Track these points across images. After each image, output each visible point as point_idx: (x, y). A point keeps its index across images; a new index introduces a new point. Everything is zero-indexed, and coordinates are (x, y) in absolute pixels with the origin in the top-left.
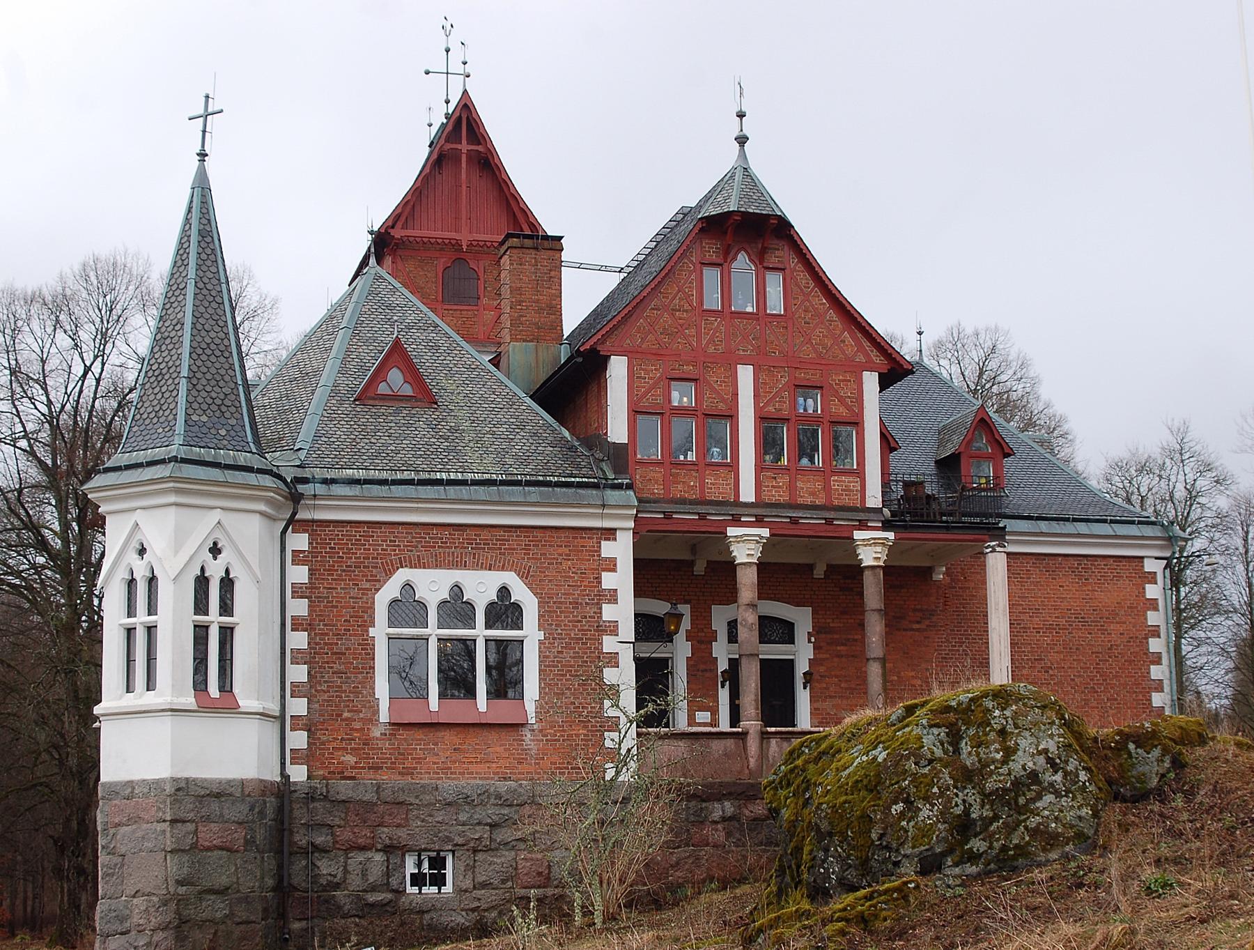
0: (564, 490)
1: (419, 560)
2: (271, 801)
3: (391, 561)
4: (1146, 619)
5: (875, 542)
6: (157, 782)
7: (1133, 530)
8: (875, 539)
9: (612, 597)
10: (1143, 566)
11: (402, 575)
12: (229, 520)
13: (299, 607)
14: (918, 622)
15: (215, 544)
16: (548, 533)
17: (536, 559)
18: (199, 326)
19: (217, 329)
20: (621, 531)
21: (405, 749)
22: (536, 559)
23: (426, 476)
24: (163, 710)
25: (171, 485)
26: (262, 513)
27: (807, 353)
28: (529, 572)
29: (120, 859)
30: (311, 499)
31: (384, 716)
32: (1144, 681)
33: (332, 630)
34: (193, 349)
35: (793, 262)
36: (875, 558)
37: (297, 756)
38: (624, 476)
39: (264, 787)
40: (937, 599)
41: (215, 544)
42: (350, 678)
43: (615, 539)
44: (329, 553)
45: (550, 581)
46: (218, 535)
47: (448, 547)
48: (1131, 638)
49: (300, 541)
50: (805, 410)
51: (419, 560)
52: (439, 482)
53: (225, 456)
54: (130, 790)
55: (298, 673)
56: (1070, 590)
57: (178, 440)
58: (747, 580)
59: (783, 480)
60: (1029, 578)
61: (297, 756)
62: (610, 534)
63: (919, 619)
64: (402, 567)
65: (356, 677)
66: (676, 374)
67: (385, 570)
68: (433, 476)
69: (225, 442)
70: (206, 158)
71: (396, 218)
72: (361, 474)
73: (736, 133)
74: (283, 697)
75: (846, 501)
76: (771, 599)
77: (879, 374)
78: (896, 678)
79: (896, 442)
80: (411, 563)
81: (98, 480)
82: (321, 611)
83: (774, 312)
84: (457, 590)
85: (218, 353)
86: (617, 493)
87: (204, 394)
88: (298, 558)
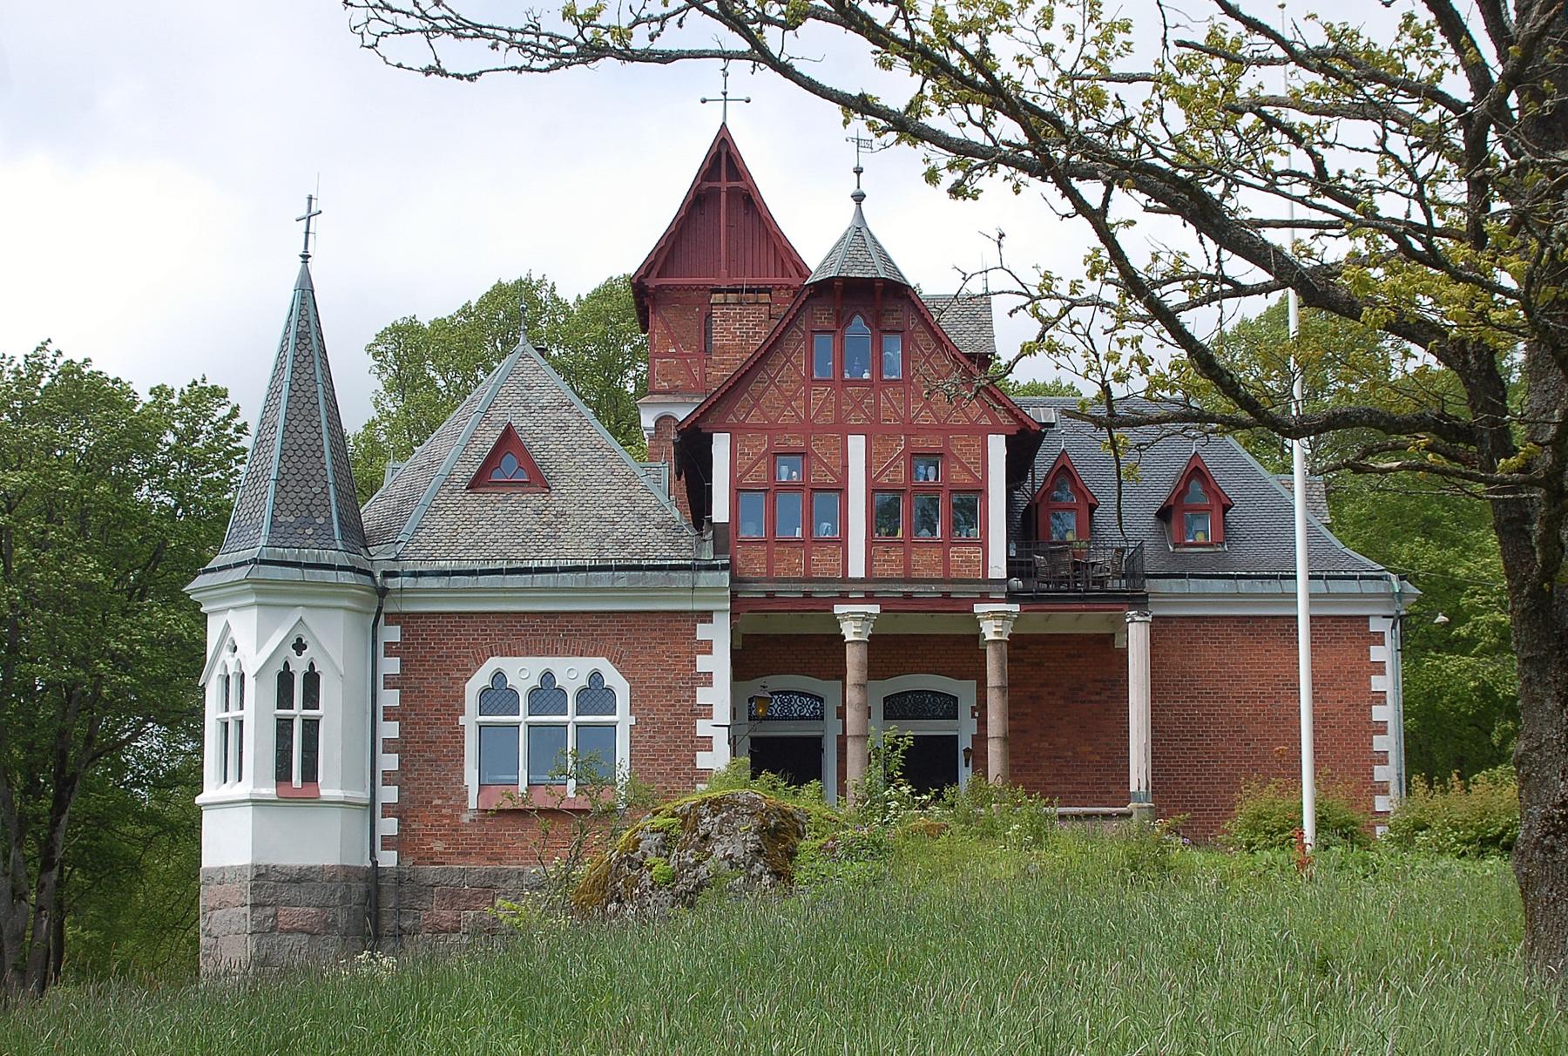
0: (656, 573)
1: (510, 649)
2: (359, 888)
3: (482, 650)
4: (1370, 684)
5: (994, 615)
6: (241, 868)
7: (1352, 587)
8: (993, 612)
9: (707, 679)
10: (1368, 626)
11: (493, 663)
12: (311, 619)
13: (391, 698)
14: (1097, 694)
15: (300, 640)
16: (642, 617)
17: (628, 643)
18: (291, 429)
19: (310, 429)
20: (720, 614)
21: (493, 835)
22: (628, 643)
23: (515, 565)
24: (244, 801)
25: (249, 586)
26: (345, 608)
27: (925, 418)
28: (621, 657)
29: (215, 940)
30: (397, 593)
31: (472, 803)
32: (1365, 752)
33: (422, 719)
34: (283, 452)
35: (913, 323)
36: (995, 632)
37: (388, 843)
38: (723, 556)
39: (348, 873)
40: (1120, 668)
41: (300, 640)
42: (440, 766)
43: (712, 622)
44: (420, 644)
45: (643, 665)
46: (300, 632)
47: (539, 635)
48: (1352, 705)
49: (393, 634)
50: (926, 478)
51: (510, 649)
52: (527, 571)
53: (308, 555)
54: (221, 875)
55: (390, 762)
56: (1279, 655)
57: (263, 542)
58: (854, 659)
59: (896, 554)
60: (1230, 643)
61: (388, 843)
62: (706, 616)
63: (1098, 690)
64: (493, 656)
65: (446, 766)
66: (782, 448)
67: (476, 659)
68: (525, 564)
69: (311, 541)
70: (309, 260)
71: (649, 266)
72: (454, 566)
73: (854, 189)
74: (373, 785)
75: (966, 573)
76: (931, 673)
77: (1007, 436)
78: (1070, 754)
79: (1094, 496)
80: (501, 650)
81: (201, 581)
82: (412, 701)
83: (894, 377)
84: (548, 676)
85: (309, 453)
86: (710, 574)
87: (292, 495)
88: (390, 649)
